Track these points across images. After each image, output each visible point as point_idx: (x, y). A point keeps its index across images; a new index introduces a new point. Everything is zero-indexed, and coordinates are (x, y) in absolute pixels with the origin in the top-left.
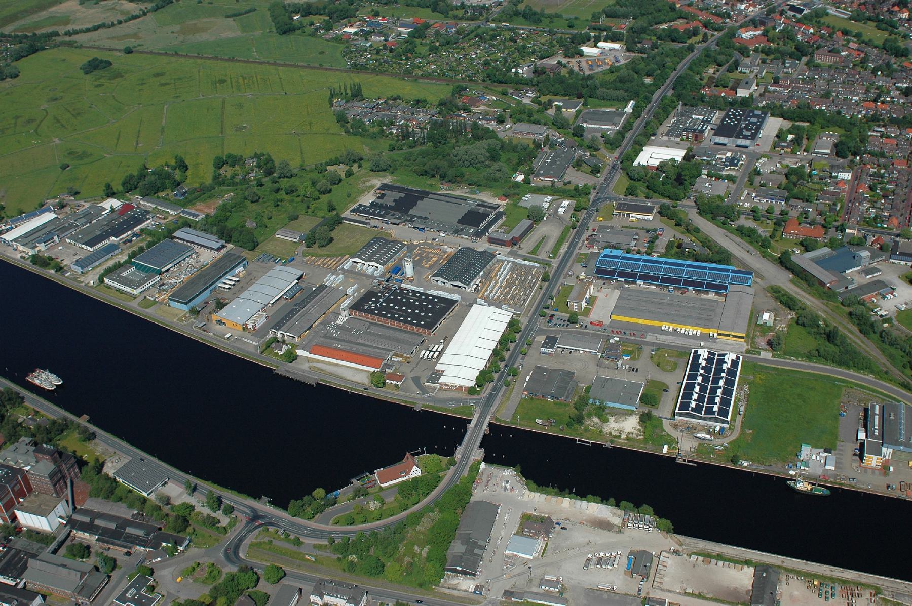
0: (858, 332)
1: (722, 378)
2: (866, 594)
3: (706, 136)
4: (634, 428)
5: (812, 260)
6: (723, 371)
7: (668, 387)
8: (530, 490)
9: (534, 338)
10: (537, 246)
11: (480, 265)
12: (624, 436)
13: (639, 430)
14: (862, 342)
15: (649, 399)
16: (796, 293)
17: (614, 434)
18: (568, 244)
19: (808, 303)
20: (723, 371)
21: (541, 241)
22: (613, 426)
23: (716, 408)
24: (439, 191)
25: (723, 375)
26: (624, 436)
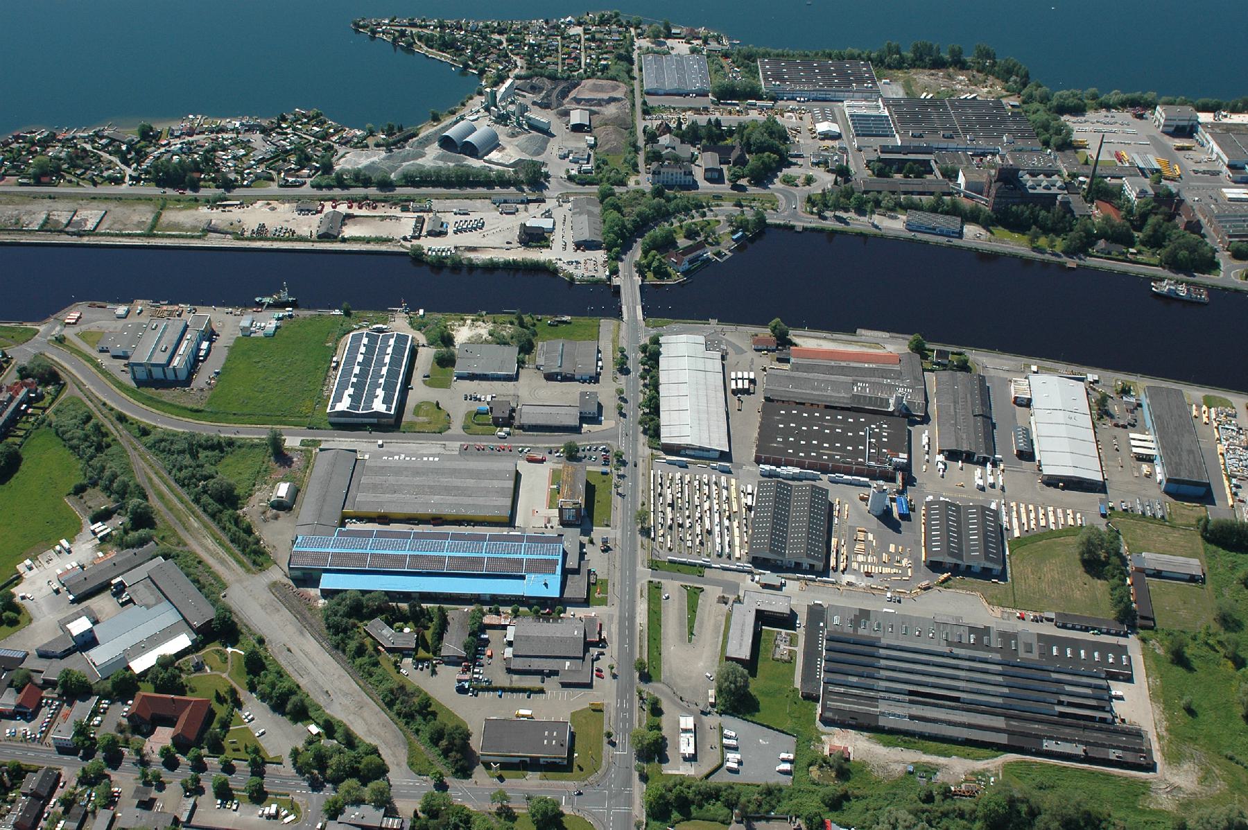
0: (150, 493)
1: (356, 376)
2: (247, 234)
3: (452, 165)
4: (458, 331)
5: (77, 335)
6: (353, 385)
7: (424, 382)
8: (550, 261)
9: (617, 423)
10: (693, 608)
11: (800, 501)
12: (469, 322)
13: (453, 330)
14: (150, 480)
15: (446, 361)
16: (222, 562)
17: (480, 323)
18: (638, 628)
19: (209, 542)
20: (353, 385)
21: (691, 628)
22: (483, 330)
23: (365, 340)
24: (1018, 763)
25: (354, 380)
26: (469, 322)
